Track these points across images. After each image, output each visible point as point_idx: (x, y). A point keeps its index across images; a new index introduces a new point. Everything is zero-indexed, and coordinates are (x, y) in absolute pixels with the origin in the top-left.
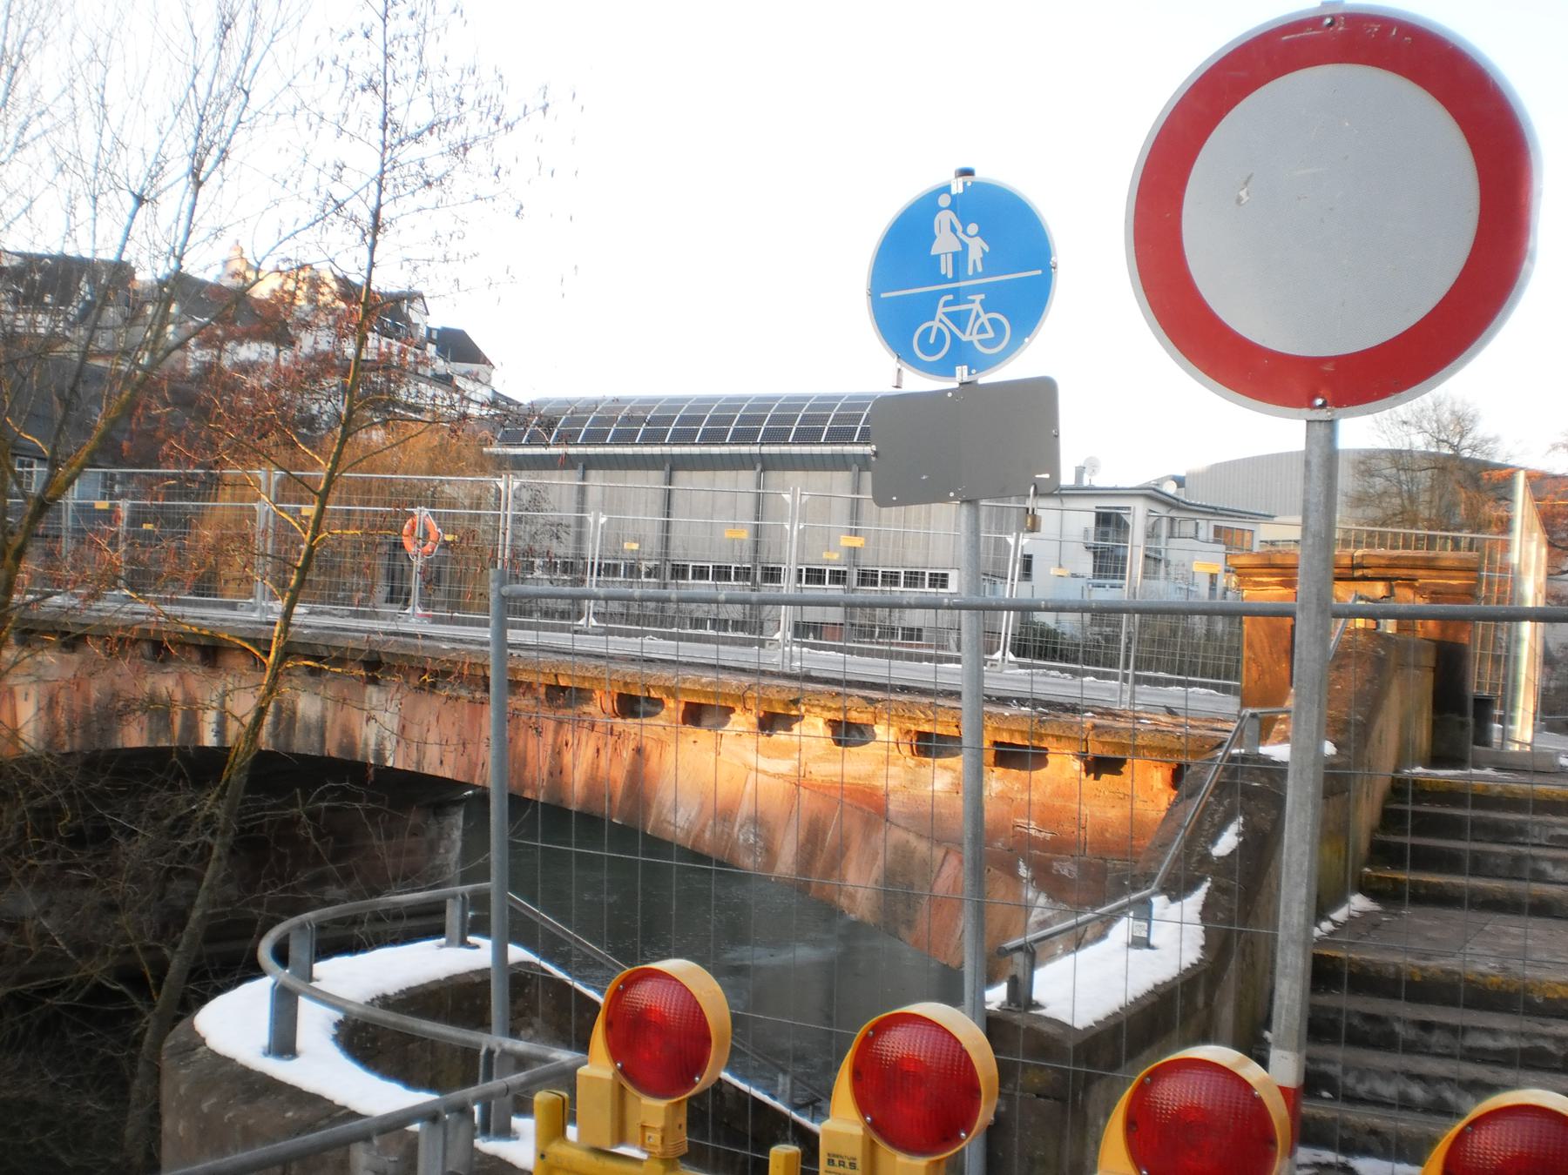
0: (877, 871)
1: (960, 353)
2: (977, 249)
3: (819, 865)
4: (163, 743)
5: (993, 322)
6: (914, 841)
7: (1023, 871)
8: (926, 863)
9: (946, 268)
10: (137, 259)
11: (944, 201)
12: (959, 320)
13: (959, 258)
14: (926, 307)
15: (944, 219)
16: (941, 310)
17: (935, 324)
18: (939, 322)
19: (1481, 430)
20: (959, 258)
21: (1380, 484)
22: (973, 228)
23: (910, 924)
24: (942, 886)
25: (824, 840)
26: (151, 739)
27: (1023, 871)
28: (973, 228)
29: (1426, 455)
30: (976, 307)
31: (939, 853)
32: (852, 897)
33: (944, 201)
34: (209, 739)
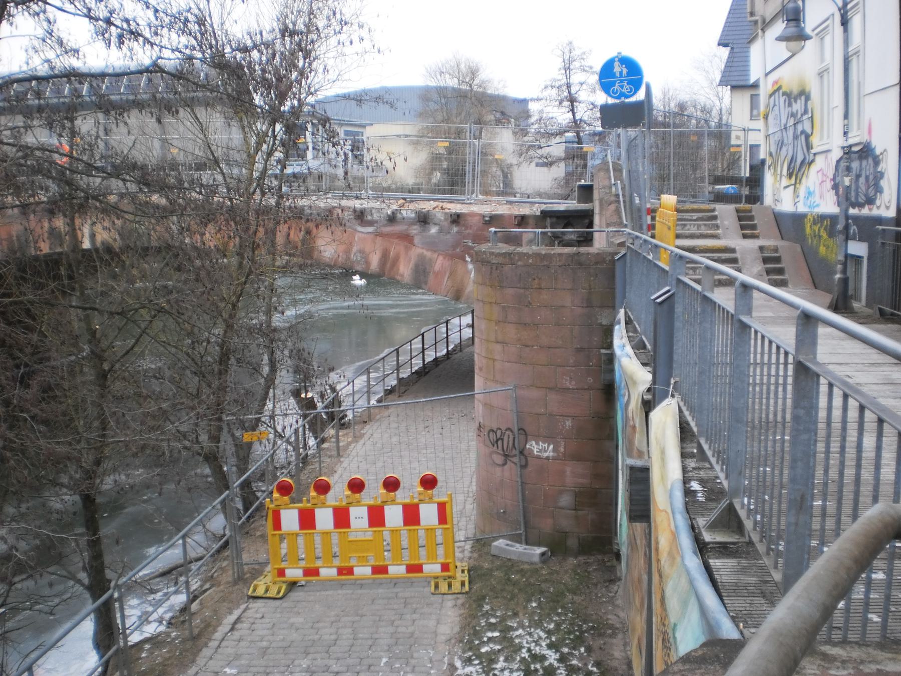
0: (412, 265)
1: (622, 95)
2: (625, 71)
3: (388, 266)
4: (59, 250)
5: (630, 88)
6: (425, 252)
7: (468, 259)
8: (430, 260)
9: (618, 75)
10: (179, 36)
11: (617, 59)
12: (622, 87)
13: (621, 73)
14: (613, 84)
15: (617, 64)
16: (617, 84)
17: (616, 88)
18: (616, 87)
19: (482, 76)
20: (621, 73)
21: (432, 106)
22: (624, 66)
23: (426, 283)
24: (437, 267)
25: (389, 255)
26: (50, 249)
27: (468, 259)
28: (624, 66)
29: (453, 89)
30: (626, 84)
31: (435, 256)
32: (402, 276)
33: (617, 59)
34: (86, 245)
